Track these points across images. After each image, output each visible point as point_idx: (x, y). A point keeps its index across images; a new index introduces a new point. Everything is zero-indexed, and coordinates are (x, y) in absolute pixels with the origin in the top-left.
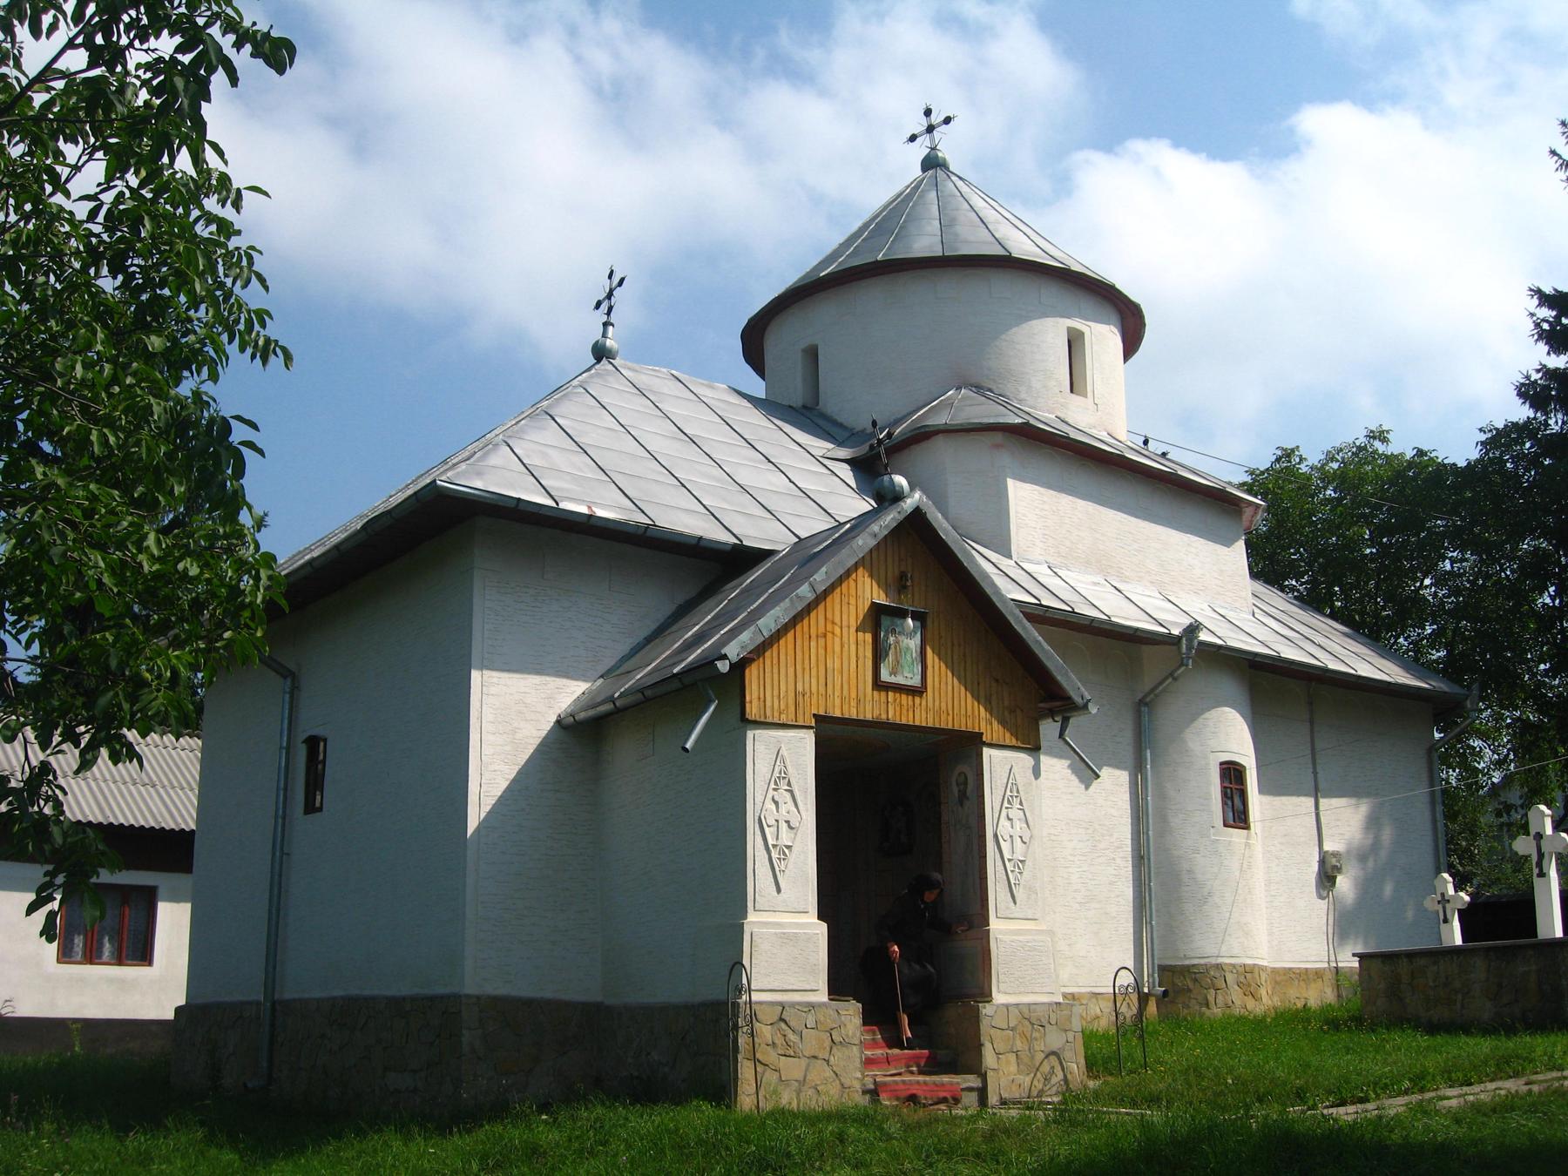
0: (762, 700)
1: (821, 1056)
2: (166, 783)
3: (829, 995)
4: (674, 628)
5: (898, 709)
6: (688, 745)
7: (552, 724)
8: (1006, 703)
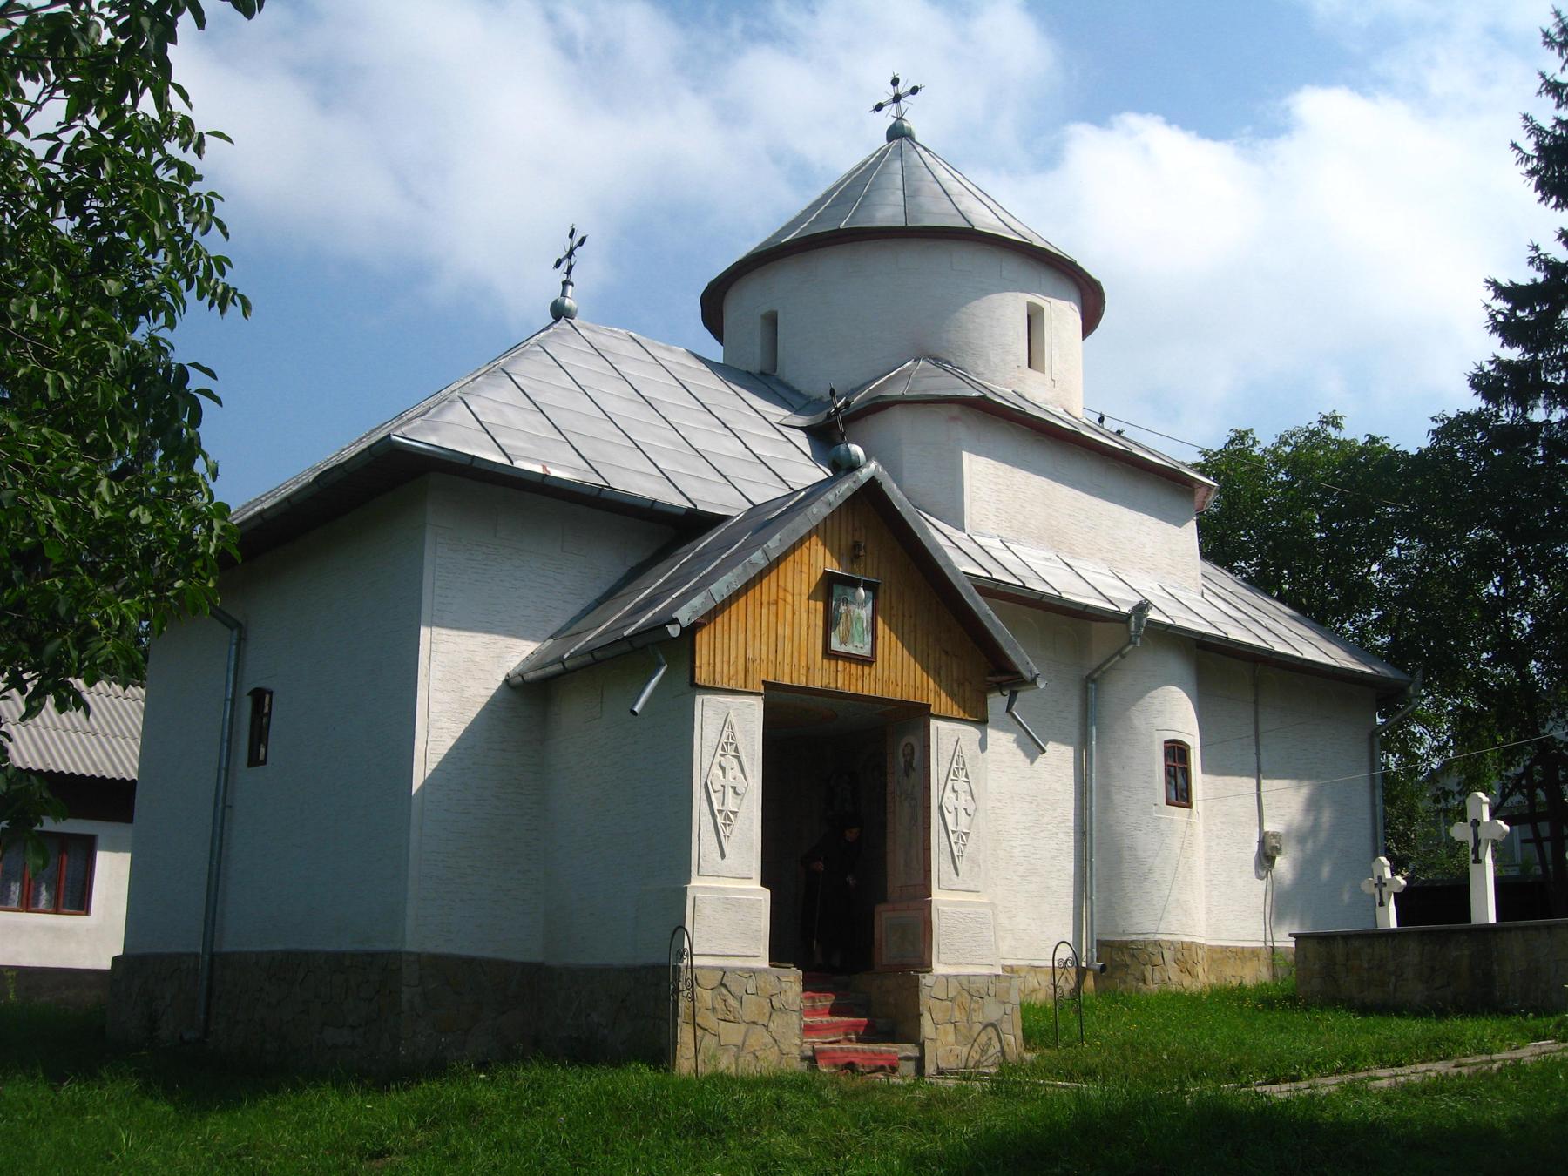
1: (760, 1023)
2: (108, 731)
4: (625, 590)
5: (847, 678)
6: (637, 709)
8: (955, 674)
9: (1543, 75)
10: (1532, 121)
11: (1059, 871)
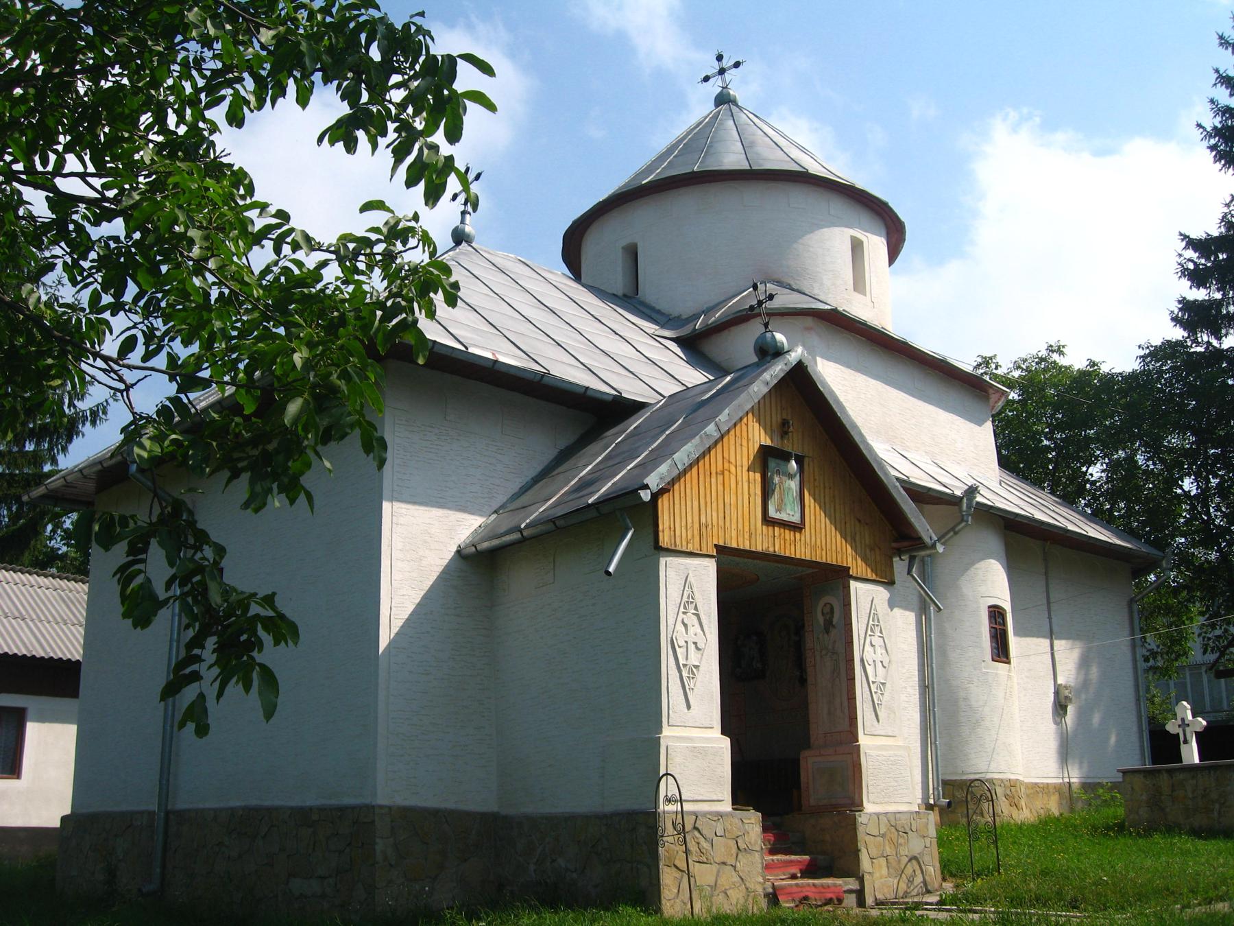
0: (672, 529)
1: (729, 863)
2: (34, 617)
3: (732, 805)
4: (561, 469)
5: (782, 542)
6: (611, 569)
7: (453, 554)
8: (867, 542)
9: (1217, 71)
10: (1218, 104)
11: (909, 720)
